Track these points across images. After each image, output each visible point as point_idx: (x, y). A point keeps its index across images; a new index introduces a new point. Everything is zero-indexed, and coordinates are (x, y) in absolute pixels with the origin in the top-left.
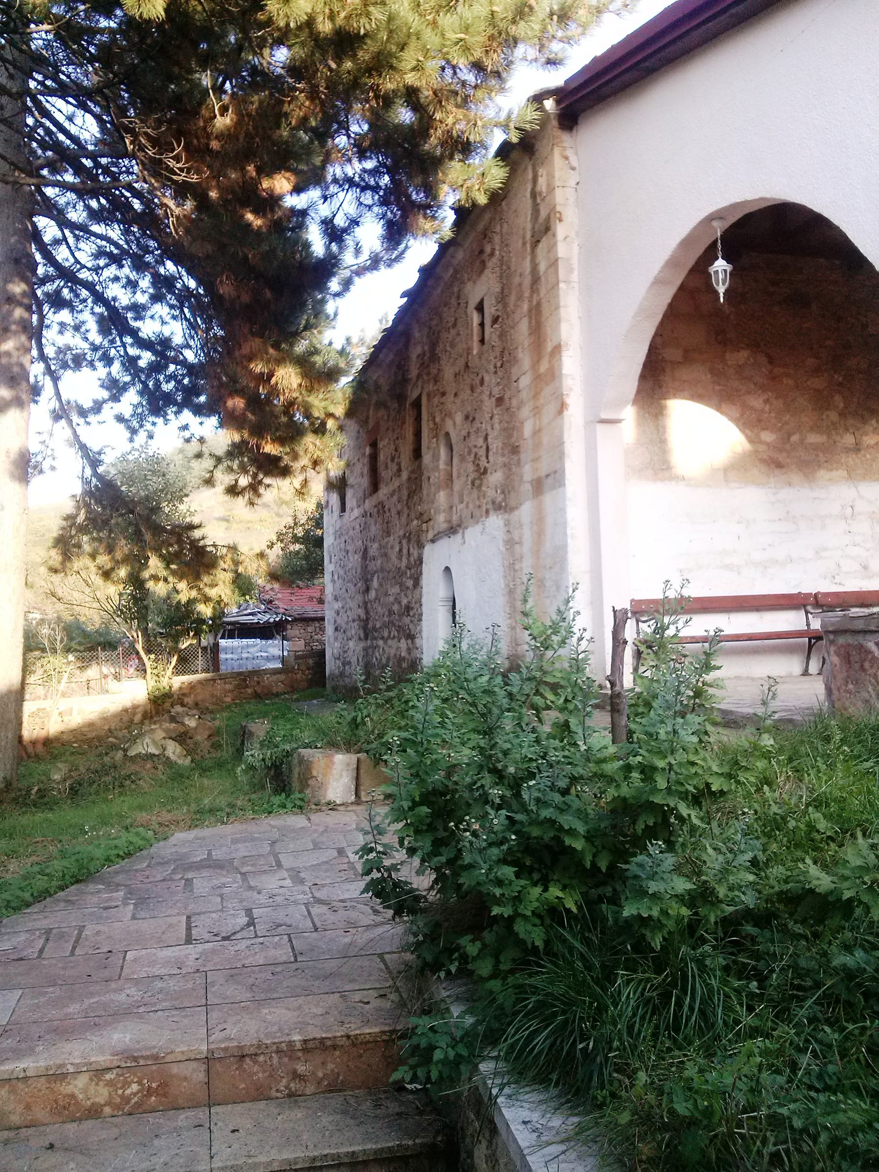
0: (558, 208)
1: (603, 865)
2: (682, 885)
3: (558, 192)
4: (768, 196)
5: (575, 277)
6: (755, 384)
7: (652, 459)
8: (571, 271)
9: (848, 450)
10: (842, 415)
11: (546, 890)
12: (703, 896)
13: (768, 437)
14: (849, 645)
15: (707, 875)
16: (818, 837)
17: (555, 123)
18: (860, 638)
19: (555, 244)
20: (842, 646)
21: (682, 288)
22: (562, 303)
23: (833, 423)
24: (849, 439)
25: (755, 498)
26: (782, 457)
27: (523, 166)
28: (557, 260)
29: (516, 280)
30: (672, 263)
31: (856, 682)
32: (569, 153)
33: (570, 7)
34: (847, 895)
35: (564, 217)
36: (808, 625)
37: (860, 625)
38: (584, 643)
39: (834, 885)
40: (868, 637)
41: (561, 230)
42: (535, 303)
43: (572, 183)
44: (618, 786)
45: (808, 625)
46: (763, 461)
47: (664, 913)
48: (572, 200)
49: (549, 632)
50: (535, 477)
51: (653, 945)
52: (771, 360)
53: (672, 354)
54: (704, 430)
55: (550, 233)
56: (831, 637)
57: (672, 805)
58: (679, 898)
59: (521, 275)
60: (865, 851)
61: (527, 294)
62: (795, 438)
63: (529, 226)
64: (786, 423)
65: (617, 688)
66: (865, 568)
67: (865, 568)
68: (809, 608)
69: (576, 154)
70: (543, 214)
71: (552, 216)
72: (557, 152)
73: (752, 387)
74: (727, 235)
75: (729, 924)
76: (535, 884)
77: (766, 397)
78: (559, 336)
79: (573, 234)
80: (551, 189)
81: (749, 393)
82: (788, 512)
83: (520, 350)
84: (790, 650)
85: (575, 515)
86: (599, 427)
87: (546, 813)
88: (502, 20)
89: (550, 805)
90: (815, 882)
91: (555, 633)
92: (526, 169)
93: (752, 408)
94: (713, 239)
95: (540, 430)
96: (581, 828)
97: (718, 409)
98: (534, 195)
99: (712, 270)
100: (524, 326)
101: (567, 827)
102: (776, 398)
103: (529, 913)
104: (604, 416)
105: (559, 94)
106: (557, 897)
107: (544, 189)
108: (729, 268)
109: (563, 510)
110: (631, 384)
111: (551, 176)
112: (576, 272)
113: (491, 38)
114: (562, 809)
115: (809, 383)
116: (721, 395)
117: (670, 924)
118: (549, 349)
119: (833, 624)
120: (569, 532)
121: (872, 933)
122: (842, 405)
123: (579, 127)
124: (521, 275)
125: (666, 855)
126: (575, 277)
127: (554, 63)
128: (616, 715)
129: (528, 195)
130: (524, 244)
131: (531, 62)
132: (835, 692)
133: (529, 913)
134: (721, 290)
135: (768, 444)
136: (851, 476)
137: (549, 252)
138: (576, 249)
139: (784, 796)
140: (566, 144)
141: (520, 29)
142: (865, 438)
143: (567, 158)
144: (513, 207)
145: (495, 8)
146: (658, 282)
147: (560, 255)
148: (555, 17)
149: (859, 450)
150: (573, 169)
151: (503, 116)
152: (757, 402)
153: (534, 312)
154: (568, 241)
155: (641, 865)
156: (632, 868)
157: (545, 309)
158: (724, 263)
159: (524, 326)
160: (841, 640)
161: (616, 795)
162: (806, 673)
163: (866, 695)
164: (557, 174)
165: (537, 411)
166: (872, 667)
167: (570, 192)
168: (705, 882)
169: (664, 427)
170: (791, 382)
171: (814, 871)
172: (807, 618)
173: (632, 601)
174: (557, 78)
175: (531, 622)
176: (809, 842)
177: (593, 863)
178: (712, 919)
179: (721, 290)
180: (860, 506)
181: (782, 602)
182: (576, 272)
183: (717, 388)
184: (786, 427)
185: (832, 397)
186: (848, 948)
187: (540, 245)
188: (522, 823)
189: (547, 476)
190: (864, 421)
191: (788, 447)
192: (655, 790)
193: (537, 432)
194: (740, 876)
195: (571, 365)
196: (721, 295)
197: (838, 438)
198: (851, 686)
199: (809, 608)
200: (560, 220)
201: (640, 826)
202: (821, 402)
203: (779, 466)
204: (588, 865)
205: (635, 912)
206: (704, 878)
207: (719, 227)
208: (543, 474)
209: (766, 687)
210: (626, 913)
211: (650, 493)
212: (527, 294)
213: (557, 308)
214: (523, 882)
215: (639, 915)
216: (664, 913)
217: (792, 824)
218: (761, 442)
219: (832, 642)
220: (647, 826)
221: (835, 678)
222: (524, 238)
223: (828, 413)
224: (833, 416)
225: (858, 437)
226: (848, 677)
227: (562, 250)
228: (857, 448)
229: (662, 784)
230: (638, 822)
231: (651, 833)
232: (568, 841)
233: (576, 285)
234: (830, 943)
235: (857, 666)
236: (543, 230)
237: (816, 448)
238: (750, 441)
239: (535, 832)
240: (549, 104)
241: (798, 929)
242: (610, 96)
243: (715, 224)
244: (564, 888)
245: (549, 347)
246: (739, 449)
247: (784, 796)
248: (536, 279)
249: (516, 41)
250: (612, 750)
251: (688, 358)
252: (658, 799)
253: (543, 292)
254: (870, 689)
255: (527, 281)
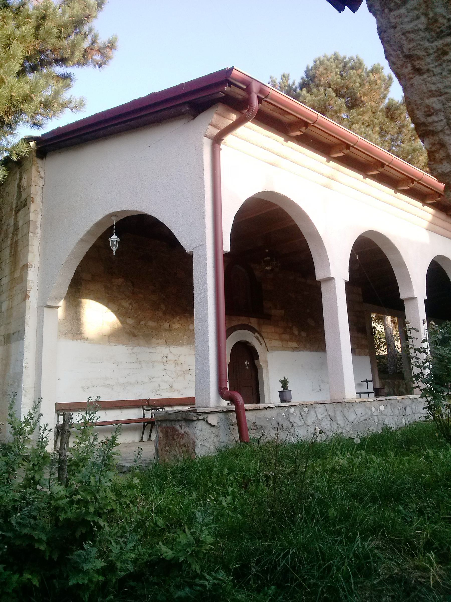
0: (32, 196)
1: (55, 557)
2: (100, 564)
3: (33, 188)
4: (139, 210)
5: (38, 231)
6: (125, 295)
7: (72, 328)
8: (37, 228)
9: (166, 330)
10: (164, 313)
11: (21, 575)
12: (110, 568)
13: (130, 321)
14: (168, 427)
15: (111, 557)
16: (158, 529)
17: (34, 154)
18: (173, 423)
19: (29, 213)
20: (164, 428)
21: (94, 246)
22: (30, 243)
23: (160, 317)
24: (166, 325)
25: (122, 351)
26: (136, 332)
27: (14, 172)
28: (29, 221)
29: (5, 228)
30: (90, 233)
31: (170, 446)
32: (40, 170)
33: (51, 102)
34: (181, 559)
35: (34, 201)
36: (144, 415)
37: (173, 417)
38: (46, 432)
39: (173, 555)
40: (177, 423)
41: (32, 207)
42: (14, 241)
43: (41, 185)
44: (66, 513)
45: (144, 415)
46: (127, 333)
47: (90, 581)
48: (39, 193)
49: (23, 425)
50: (6, 334)
51: (84, 599)
52: (133, 285)
53: (86, 276)
54: (98, 316)
55: (26, 207)
56: (159, 423)
57: (96, 520)
58: (98, 572)
59: (8, 225)
60: (189, 536)
61: (10, 236)
62: (142, 323)
63: (15, 202)
64: (139, 315)
65: (63, 457)
66: (171, 387)
67: (171, 387)
68: (145, 407)
69: (44, 171)
70: (23, 197)
71: (28, 199)
72: (34, 168)
73: (124, 296)
74: (119, 224)
75: (122, 582)
76: (14, 573)
77: (130, 302)
78: (27, 259)
79: (39, 210)
80: (29, 186)
81: (122, 299)
82: (137, 359)
83: (4, 264)
84: (134, 429)
85: (29, 356)
86: (45, 309)
87: (26, 531)
88: (16, 100)
89: (27, 526)
90: (165, 554)
91: (27, 426)
92: (16, 173)
93: (123, 306)
94: (111, 225)
95: (12, 308)
96: (44, 538)
97: (107, 306)
98: (19, 186)
99: (110, 240)
100: (7, 252)
101: (36, 538)
102: (135, 303)
103: (10, 591)
104: (49, 304)
105: (37, 140)
106: (28, 579)
107: (25, 185)
108: (118, 240)
109: (22, 353)
110: (64, 290)
111: (30, 180)
112: (39, 229)
113: (9, 107)
114: (33, 528)
115: (150, 297)
116: (108, 299)
117: (93, 586)
118: (21, 266)
119: (161, 417)
120: (24, 365)
121: (189, 577)
122: (164, 309)
123: (47, 158)
124: (8, 225)
125: (93, 549)
126: (38, 231)
127: (37, 126)
128: (61, 472)
129: (16, 186)
130: (11, 210)
131: (25, 122)
132: (160, 451)
133: (10, 591)
134: (114, 250)
135: (130, 325)
136: (167, 343)
137: (25, 216)
138: (40, 218)
139: (140, 508)
140: (39, 165)
141: (25, 107)
142: (173, 325)
143: (39, 172)
144: (6, 191)
145: (13, 94)
146: (82, 240)
147: (31, 219)
148: (42, 105)
149: (171, 330)
150: (42, 178)
151: (10, 146)
152: (125, 304)
153: (13, 245)
154: (36, 213)
155: (79, 556)
156: (73, 557)
157: (20, 243)
158: (116, 237)
159: (7, 252)
160: (164, 425)
161: (65, 517)
162: (141, 441)
163: (175, 453)
164: (33, 179)
165: (11, 298)
166: (178, 438)
167: (39, 189)
168: (111, 561)
169: (80, 312)
170: (142, 296)
171: (164, 549)
172: (144, 412)
173: (56, 404)
174: (38, 133)
175: (13, 419)
176: (156, 533)
177: (50, 557)
178: (114, 581)
179: (114, 250)
180: (171, 357)
181: (132, 404)
182: (39, 229)
183: (107, 295)
184: (139, 317)
185: (160, 305)
186: (178, 587)
187: (20, 212)
188: (10, 537)
189: (14, 333)
190: (174, 317)
191: (139, 327)
192: (88, 513)
193: (10, 309)
194: (128, 556)
195: (33, 276)
196: (114, 252)
197: (162, 324)
198: (167, 448)
199: (145, 407)
200: (33, 202)
201: (78, 534)
202: (155, 307)
203: (135, 336)
204: (47, 558)
205: (75, 582)
206: (110, 559)
207: (114, 220)
208: (12, 332)
209: (137, 452)
210: (70, 583)
211: (70, 346)
212: (10, 236)
213: (27, 245)
214: (8, 573)
215: (78, 584)
216: (90, 581)
217: (148, 523)
218: (127, 324)
219: (160, 426)
220: (82, 533)
221: (160, 444)
222: (11, 207)
223: (157, 312)
224: (160, 314)
225: (171, 324)
226: (166, 443)
227: (32, 217)
228: (170, 329)
229: (92, 510)
230: (73, 531)
231: (84, 538)
232: (37, 546)
233: (38, 236)
234: (169, 585)
235: (171, 438)
236: (23, 204)
237: (153, 328)
238: (122, 323)
239: (18, 542)
240: (32, 144)
241: (155, 580)
242: (63, 147)
243: (113, 218)
244: (31, 574)
245: (21, 264)
246: (116, 326)
247: (140, 508)
248: (16, 229)
249: (22, 112)
250: (63, 493)
251: (94, 279)
252: (89, 518)
253: (20, 236)
254: (177, 449)
255: (11, 229)
